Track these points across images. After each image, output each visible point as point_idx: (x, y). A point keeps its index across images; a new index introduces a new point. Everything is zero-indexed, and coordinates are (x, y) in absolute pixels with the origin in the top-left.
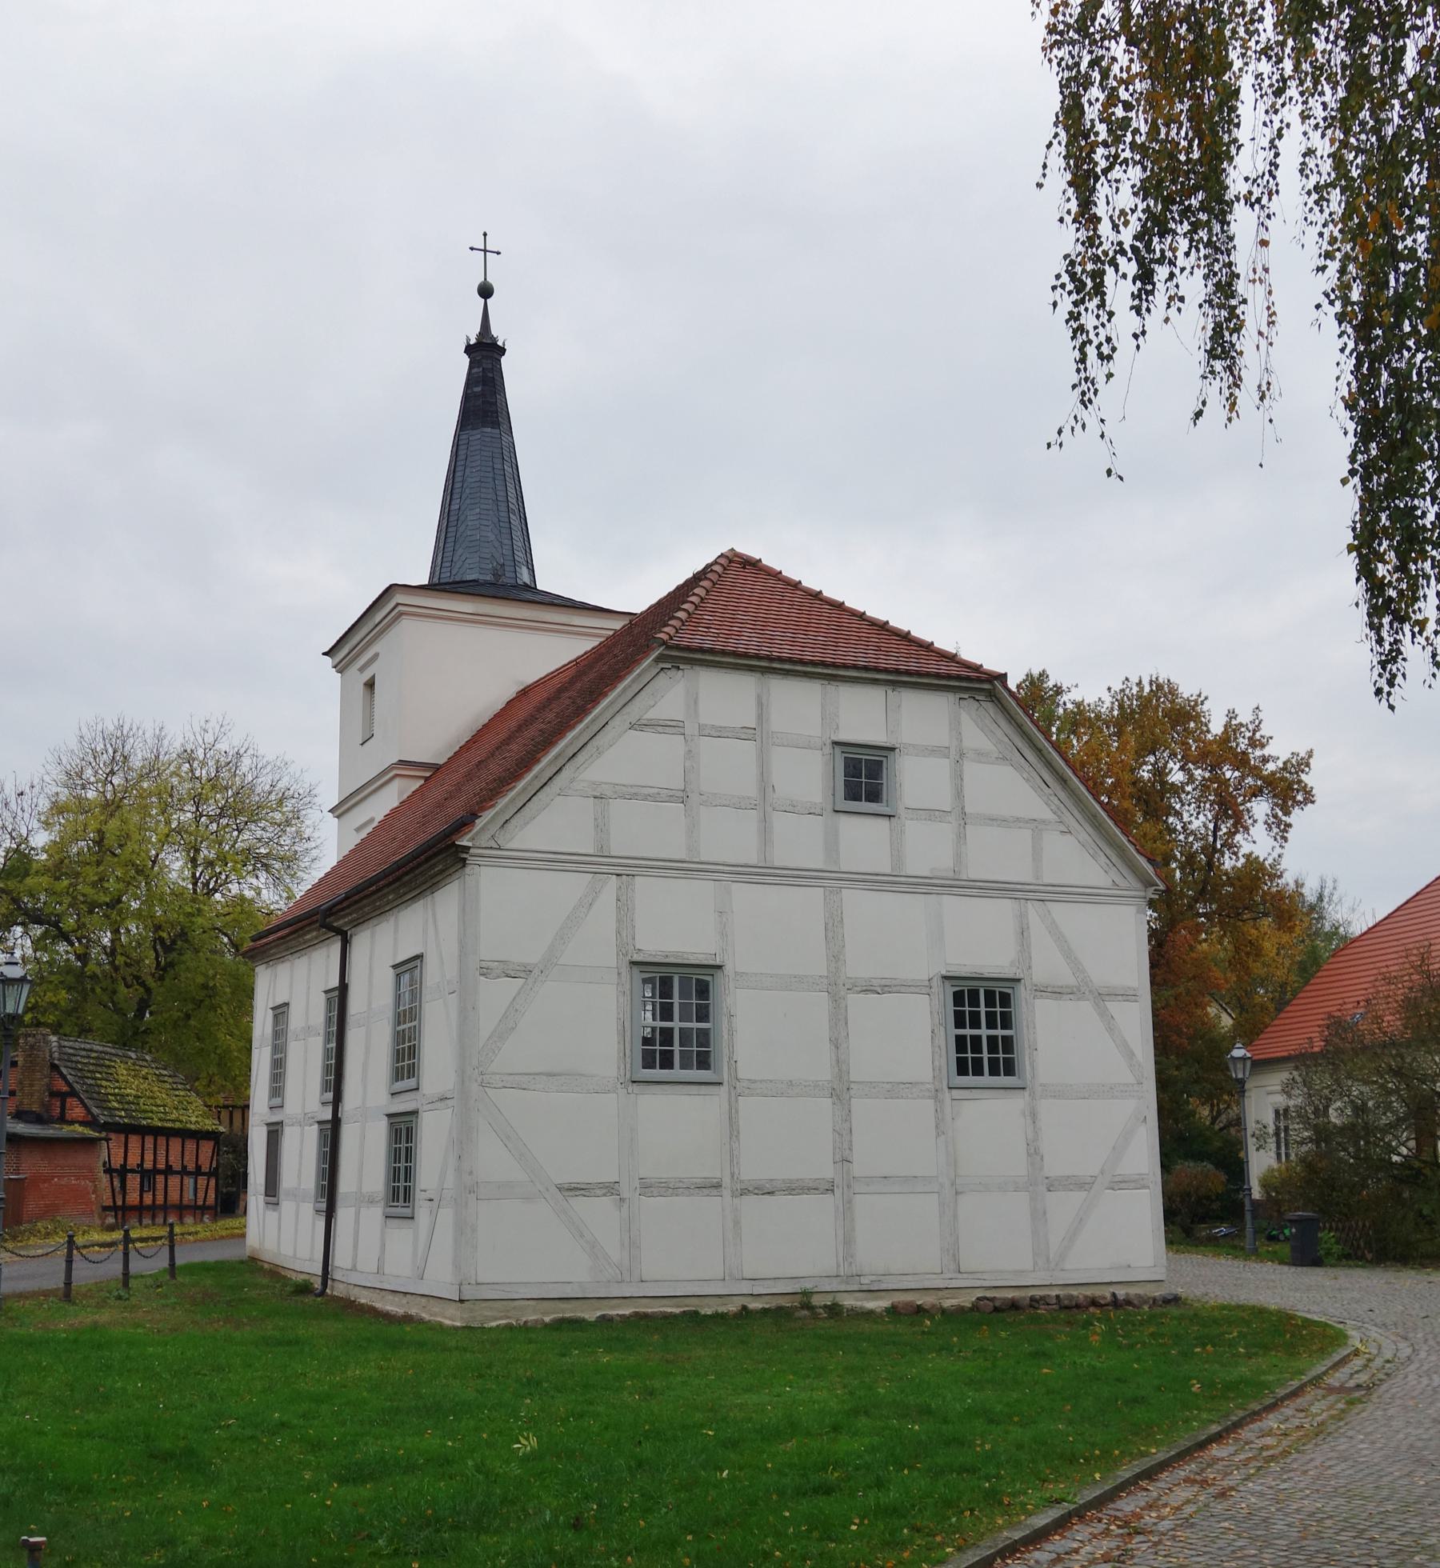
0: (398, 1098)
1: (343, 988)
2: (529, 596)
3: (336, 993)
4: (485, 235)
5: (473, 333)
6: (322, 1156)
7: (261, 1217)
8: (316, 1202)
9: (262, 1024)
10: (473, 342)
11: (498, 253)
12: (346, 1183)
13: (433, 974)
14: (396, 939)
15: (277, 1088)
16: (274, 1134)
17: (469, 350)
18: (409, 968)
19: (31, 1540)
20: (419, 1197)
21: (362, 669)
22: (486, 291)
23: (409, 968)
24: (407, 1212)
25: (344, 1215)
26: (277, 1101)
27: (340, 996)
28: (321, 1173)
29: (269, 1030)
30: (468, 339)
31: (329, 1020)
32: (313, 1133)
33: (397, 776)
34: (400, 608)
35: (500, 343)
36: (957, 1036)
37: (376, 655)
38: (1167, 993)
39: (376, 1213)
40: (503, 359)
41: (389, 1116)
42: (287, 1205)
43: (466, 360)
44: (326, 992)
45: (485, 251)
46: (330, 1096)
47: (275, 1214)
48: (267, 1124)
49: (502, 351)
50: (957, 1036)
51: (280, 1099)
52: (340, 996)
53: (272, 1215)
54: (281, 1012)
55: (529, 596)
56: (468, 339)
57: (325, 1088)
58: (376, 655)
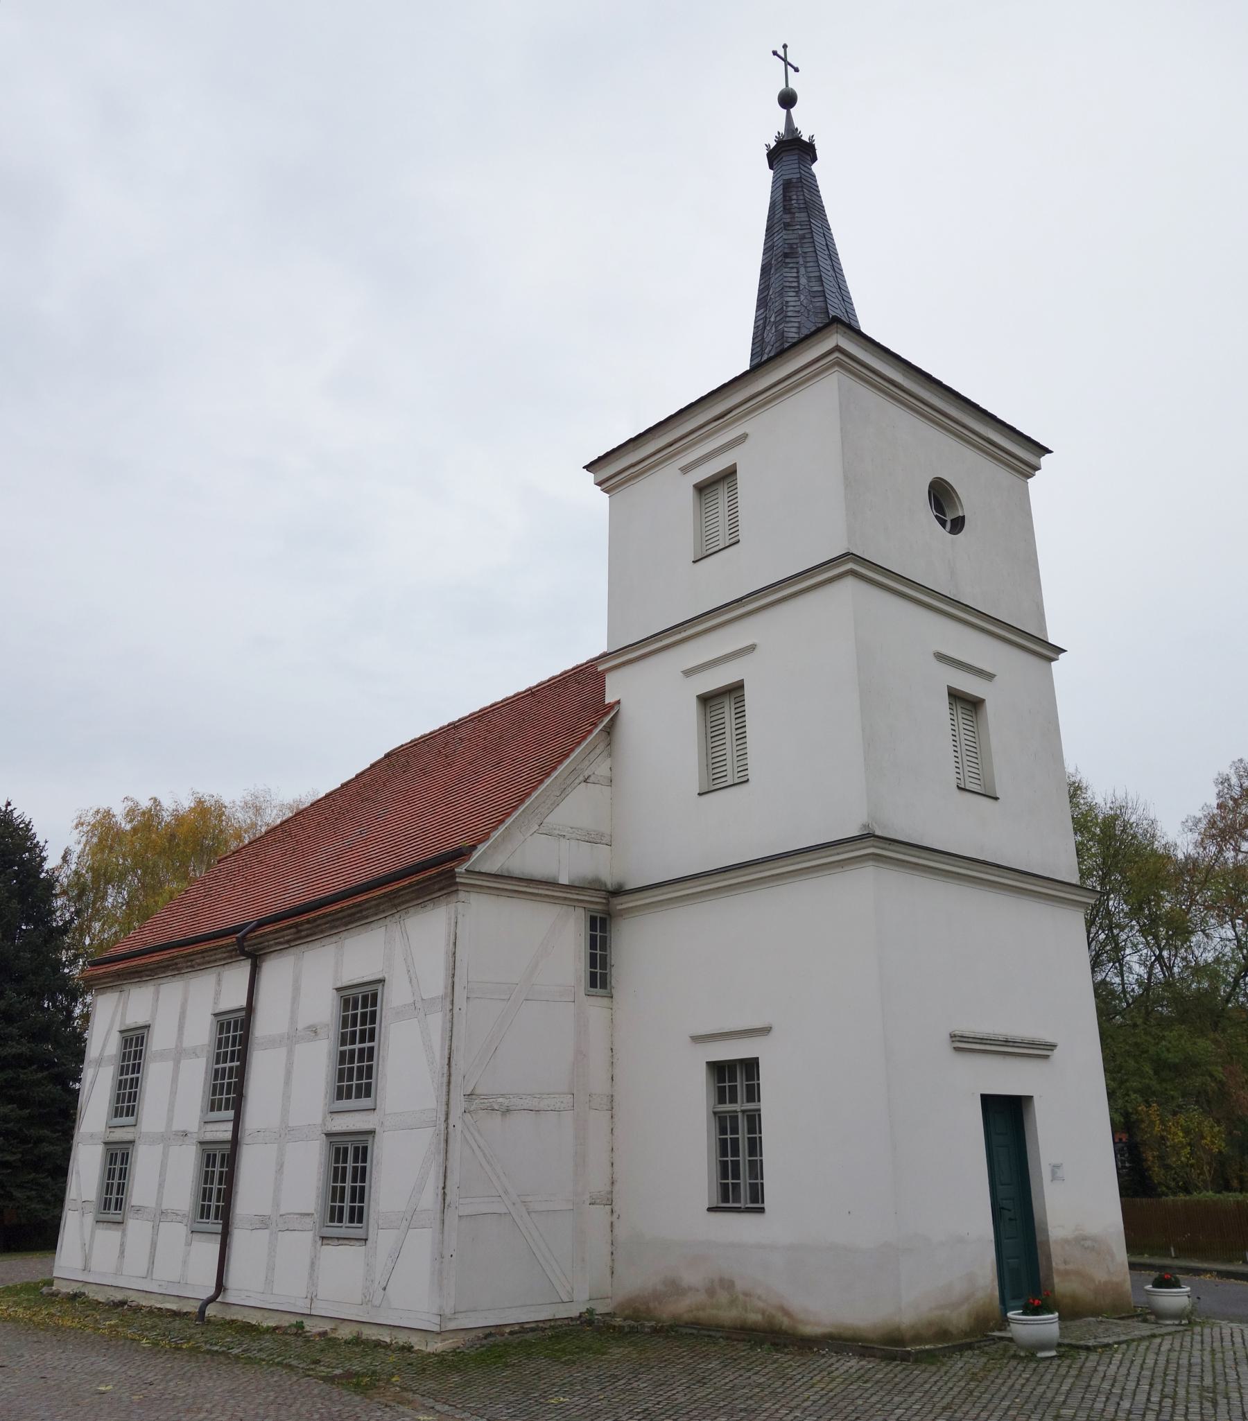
10: (773, 144)
21: (685, 470)
22: (788, 100)
37: (743, 438)
39: (89, 1219)
42: (137, 1228)
48: (106, 1143)
58: (743, 438)
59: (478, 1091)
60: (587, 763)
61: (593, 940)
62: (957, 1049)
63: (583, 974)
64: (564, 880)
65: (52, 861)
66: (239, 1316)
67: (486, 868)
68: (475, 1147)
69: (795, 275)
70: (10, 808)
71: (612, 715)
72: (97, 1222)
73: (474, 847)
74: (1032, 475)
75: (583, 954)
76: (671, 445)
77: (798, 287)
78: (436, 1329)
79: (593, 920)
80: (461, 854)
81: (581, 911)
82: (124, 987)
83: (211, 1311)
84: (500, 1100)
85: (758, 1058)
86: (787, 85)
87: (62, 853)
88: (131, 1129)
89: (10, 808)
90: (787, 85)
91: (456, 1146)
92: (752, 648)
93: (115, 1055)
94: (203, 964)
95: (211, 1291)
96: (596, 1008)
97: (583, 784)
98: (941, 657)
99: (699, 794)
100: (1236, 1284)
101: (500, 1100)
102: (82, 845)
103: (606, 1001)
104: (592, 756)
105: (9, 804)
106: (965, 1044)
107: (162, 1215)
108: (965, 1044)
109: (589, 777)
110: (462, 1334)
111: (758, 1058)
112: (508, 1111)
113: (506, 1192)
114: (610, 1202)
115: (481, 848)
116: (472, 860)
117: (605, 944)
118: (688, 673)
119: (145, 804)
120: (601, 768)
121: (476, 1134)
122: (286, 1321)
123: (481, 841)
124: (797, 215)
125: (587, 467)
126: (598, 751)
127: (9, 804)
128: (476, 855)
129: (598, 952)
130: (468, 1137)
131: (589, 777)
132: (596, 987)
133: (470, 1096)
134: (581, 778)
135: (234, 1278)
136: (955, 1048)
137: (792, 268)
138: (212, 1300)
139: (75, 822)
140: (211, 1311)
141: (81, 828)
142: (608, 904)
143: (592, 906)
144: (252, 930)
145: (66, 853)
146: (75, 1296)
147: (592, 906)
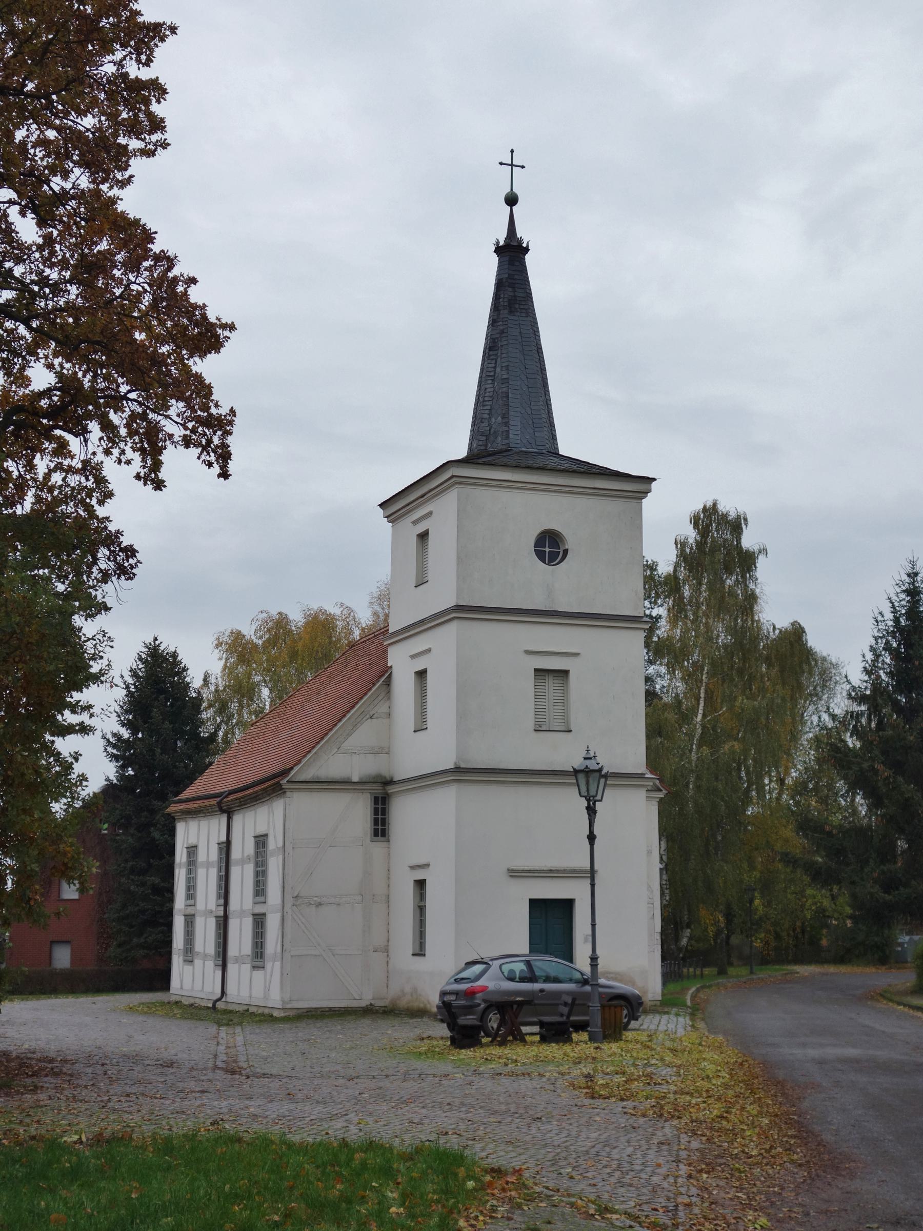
0: (257, 906)
1: (228, 843)
3: (225, 845)
4: (512, 151)
5: (502, 237)
6: (218, 935)
7: (181, 969)
8: (215, 960)
9: (181, 856)
10: (502, 243)
12: (232, 951)
13: (273, 843)
14: (255, 822)
15: (191, 895)
16: (190, 920)
17: (499, 250)
18: (261, 841)
20: (267, 957)
21: (415, 523)
22: (511, 200)
23: (261, 841)
24: (261, 964)
25: (231, 968)
26: (191, 902)
27: (226, 847)
28: (218, 945)
29: (184, 859)
30: (498, 242)
31: (220, 859)
32: (212, 923)
34: (454, 479)
36: (534, 904)
37: (430, 514)
39: (247, 967)
41: (254, 915)
42: (198, 962)
44: (219, 844)
46: (222, 901)
47: (190, 968)
48: (185, 915)
50: (534, 904)
51: (193, 901)
52: (226, 847)
53: (188, 968)
54: (192, 850)
57: (219, 897)
58: (430, 514)
60: (372, 706)
61: (376, 811)
62: (511, 876)
63: (369, 830)
64: (355, 779)
65: (195, 679)
66: (231, 1007)
67: (302, 778)
68: (299, 922)
69: (493, 365)
70: (157, 643)
71: (386, 675)
72: (254, 967)
73: (292, 768)
74: (646, 493)
76: (408, 505)
77: (494, 375)
78: (281, 1007)
79: (376, 800)
80: (285, 772)
81: (368, 795)
82: (188, 820)
83: (220, 1005)
85: (531, 900)
86: (512, 190)
87: (202, 677)
88: (193, 907)
89: (157, 643)
90: (512, 190)
91: (288, 923)
92: (429, 650)
94: (212, 812)
95: (219, 994)
96: (378, 848)
97: (369, 720)
98: (528, 652)
99: (415, 731)
100: (913, 1017)
102: (224, 660)
103: (385, 844)
104: (376, 702)
105: (156, 639)
106: (515, 874)
107: (205, 956)
108: (515, 874)
110: (295, 1011)
111: (531, 900)
112: (319, 905)
113: (319, 945)
114: (386, 950)
115: (296, 769)
116: (290, 776)
117: (384, 812)
118: (413, 657)
120: (382, 708)
121: (301, 917)
122: (241, 1008)
123: (295, 765)
124: (501, 312)
125: (380, 505)
126: (380, 698)
127: (156, 639)
128: (292, 773)
129: (380, 817)
130: (295, 917)
134: (368, 716)
135: (231, 989)
136: (511, 876)
137: (492, 359)
138: (219, 1000)
139: (216, 642)
140: (220, 1005)
141: (220, 648)
142: (385, 789)
144: (226, 797)
145: (205, 676)
146: (177, 1003)
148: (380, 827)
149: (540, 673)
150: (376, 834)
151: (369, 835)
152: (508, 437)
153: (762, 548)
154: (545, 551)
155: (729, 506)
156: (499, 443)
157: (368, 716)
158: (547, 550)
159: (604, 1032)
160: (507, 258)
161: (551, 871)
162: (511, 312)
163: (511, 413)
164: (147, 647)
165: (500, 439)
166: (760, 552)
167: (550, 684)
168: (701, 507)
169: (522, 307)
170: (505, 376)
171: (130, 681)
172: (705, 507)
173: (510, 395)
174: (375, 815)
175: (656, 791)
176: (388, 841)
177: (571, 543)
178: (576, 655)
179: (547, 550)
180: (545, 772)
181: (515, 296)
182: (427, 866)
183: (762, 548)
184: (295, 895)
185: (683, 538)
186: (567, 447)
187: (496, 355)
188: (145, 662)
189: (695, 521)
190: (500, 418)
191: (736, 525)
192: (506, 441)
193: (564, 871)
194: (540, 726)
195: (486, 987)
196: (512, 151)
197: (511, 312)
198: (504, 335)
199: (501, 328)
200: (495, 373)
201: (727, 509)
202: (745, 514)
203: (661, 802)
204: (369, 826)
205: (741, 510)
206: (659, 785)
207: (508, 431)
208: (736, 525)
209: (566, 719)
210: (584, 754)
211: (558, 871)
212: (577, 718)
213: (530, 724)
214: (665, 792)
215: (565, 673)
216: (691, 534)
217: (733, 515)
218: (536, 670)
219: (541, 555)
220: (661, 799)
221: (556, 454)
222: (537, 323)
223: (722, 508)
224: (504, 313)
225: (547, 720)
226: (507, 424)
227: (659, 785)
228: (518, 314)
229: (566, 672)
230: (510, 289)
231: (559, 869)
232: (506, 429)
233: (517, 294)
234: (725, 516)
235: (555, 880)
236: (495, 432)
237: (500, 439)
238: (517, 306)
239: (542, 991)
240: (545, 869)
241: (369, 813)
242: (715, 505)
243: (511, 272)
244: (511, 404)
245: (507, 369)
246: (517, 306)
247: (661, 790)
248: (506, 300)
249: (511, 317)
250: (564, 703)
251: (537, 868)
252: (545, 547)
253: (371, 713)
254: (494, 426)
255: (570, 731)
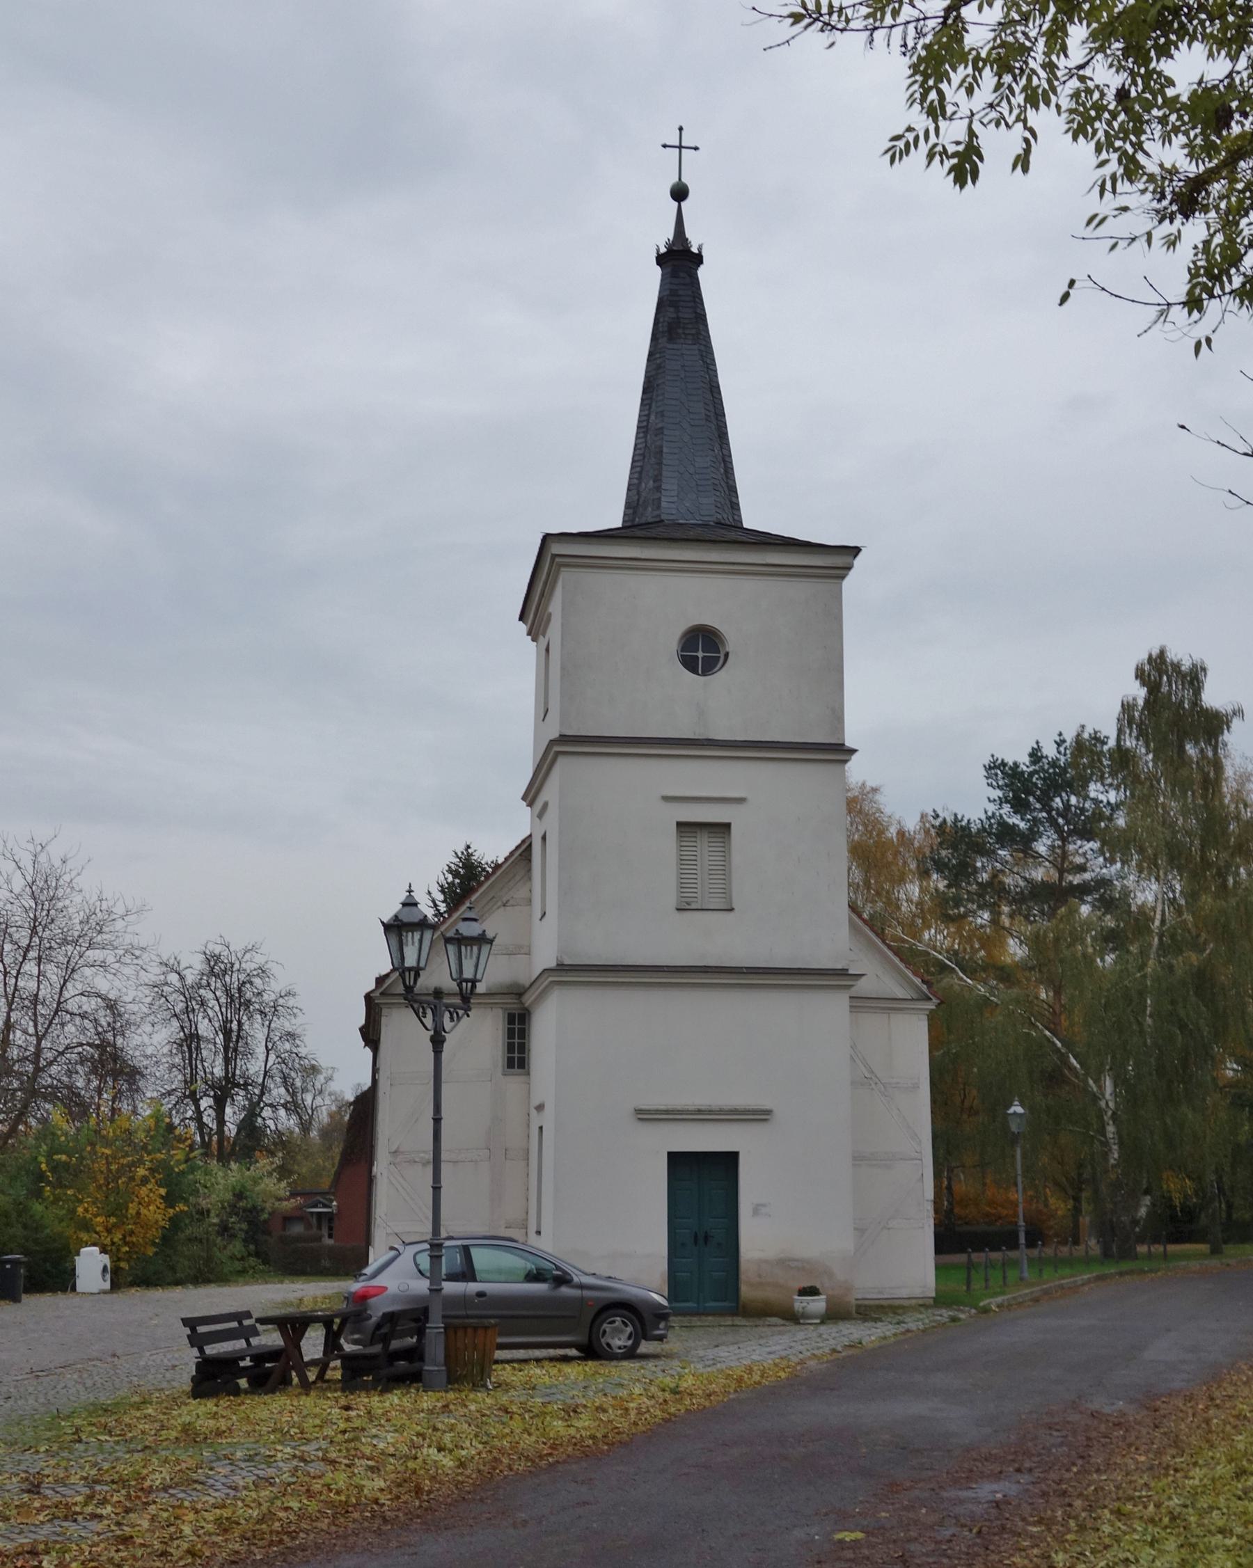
2: (733, 535)
4: (681, 129)
10: (663, 250)
11: (696, 149)
17: (661, 260)
19: (1078, 1066)
22: (680, 193)
33: (558, 753)
35: (694, 250)
36: (675, 1159)
38: (937, 1054)
40: (702, 272)
43: (658, 271)
45: (680, 147)
49: (698, 259)
50: (675, 1159)
55: (733, 535)
56: (658, 250)
59: (401, 1150)
61: (511, 1034)
70: (470, 851)
75: (500, 1044)
77: (647, 426)
79: (511, 1019)
81: (500, 1011)
84: (422, 1155)
85: (670, 1154)
86: (680, 179)
90: (680, 179)
93: (844, 745)
96: (513, 1083)
97: (503, 908)
98: (667, 799)
101: (422, 1155)
103: (523, 1078)
105: (468, 847)
106: (645, 1116)
108: (645, 1116)
109: (508, 901)
111: (670, 1154)
119: (1214, 696)
120: (520, 893)
121: (401, 1179)
126: (518, 878)
131: (508, 901)
132: (514, 1067)
133: (395, 1153)
134: (499, 903)
143: (508, 1006)
147: (508, 1006)
148: (516, 1055)
149: (685, 828)
150: (510, 1064)
151: (500, 1064)
152: (659, 507)
153: (1236, 708)
154: (697, 657)
155: (1182, 653)
156: (649, 515)
157: (499, 903)
158: (700, 654)
159: (449, 1372)
160: (669, 270)
161: (699, 1111)
162: (671, 340)
163: (664, 473)
164: (457, 856)
165: (650, 509)
166: (1234, 714)
167: (704, 846)
168: (1146, 657)
169: (687, 332)
170: (660, 425)
171: (439, 897)
172: (1150, 657)
173: (665, 450)
174: (509, 1038)
175: (923, 1000)
176: (529, 1074)
177: (733, 640)
178: (741, 800)
179: (700, 654)
180: (693, 969)
181: (678, 318)
182: (760, 1116)
183: (1236, 708)
184: (394, 1149)
185: (1130, 699)
186: (753, 518)
187: (651, 398)
188: (455, 874)
189: (1140, 674)
190: (651, 482)
191: (1194, 678)
192: (656, 513)
193: (721, 1112)
194: (688, 904)
195: (385, 1289)
196: (681, 129)
197: (671, 340)
198: (660, 371)
199: (658, 361)
200: (648, 421)
201: (1179, 657)
202: (1203, 662)
203: (932, 1018)
204: (500, 1053)
205: (1197, 657)
206: (927, 992)
207: (659, 499)
208: (1194, 678)
209: (727, 893)
210: (403, 896)
211: (710, 1112)
212: (742, 890)
213: (671, 900)
214: (935, 1001)
215: (726, 827)
216: (1139, 693)
217: (1186, 665)
218: (679, 824)
219: (690, 664)
220: (931, 1011)
221: (738, 526)
222: (712, 353)
223: (1172, 656)
224: (663, 341)
225: (698, 895)
226: (658, 489)
227: (927, 992)
228: (682, 341)
229: (727, 826)
230: (672, 309)
231: (713, 1108)
232: (657, 495)
233: (681, 315)
234: (1176, 666)
235: (662, 1125)
236: (644, 501)
237: (650, 509)
238: (680, 331)
239: (481, 1294)
240: (691, 1108)
241: (501, 1037)
242: (1162, 653)
243: (675, 287)
244: (664, 462)
245: (663, 416)
246: (680, 331)
247: (931, 999)
248: (666, 324)
249: (670, 346)
250: (725, 870)
251: (679, 1108)
252: (697, 651)
253: (505, 900)
254: (644, 494)
255: (732, 910)
